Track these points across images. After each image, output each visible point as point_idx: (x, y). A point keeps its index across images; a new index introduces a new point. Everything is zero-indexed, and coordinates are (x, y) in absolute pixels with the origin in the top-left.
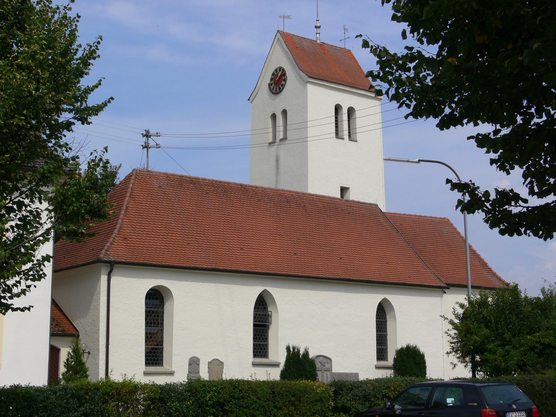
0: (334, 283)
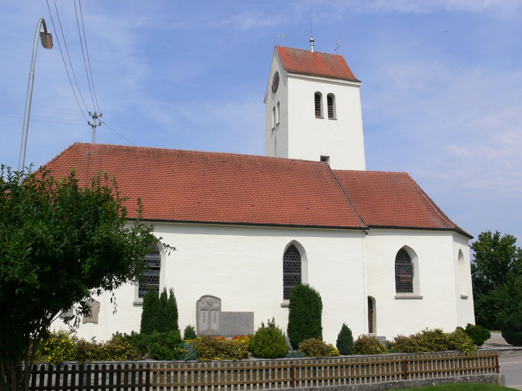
0: (234, 227)
